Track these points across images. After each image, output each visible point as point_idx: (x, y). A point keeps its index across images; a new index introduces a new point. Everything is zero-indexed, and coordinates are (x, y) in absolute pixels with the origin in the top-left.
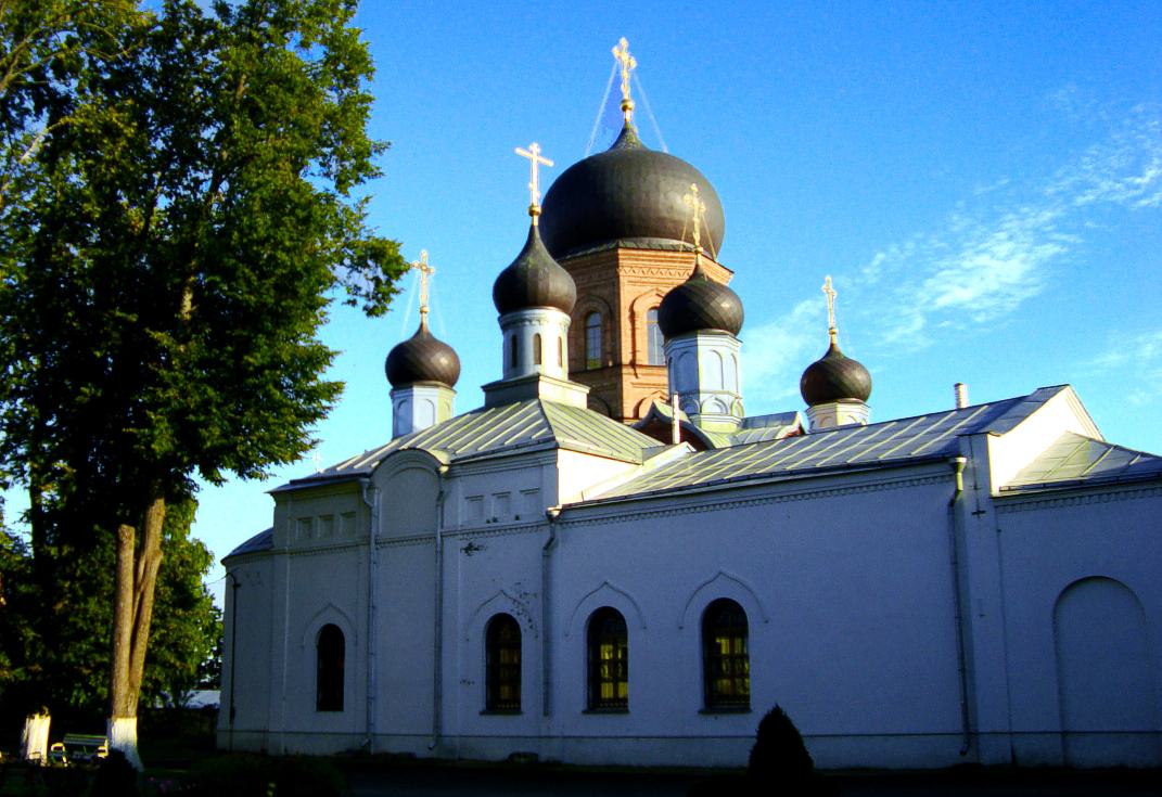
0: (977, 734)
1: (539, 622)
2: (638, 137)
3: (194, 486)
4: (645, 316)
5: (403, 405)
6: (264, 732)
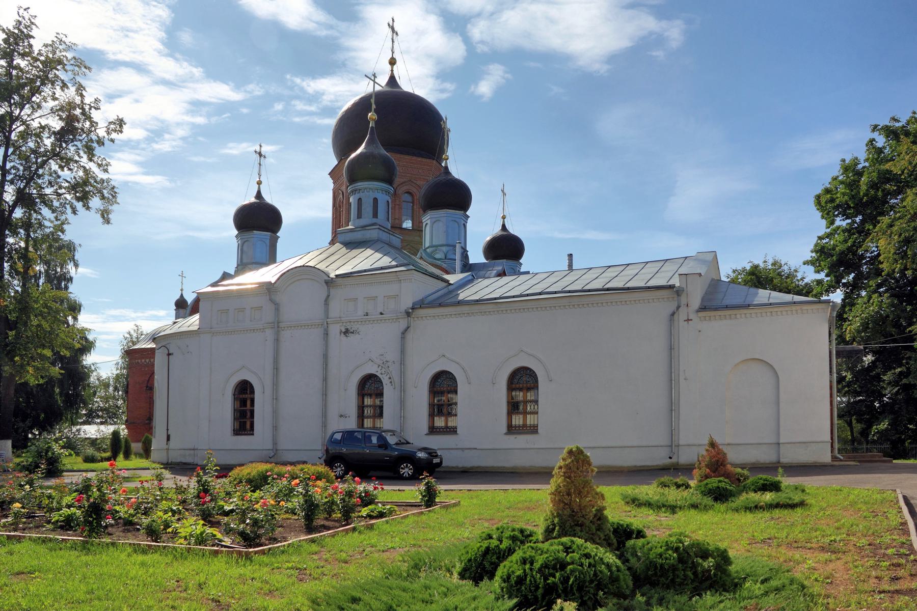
1: (396, 379)
3: (818, 272)
5: (246, 243)
6: (194, 449)
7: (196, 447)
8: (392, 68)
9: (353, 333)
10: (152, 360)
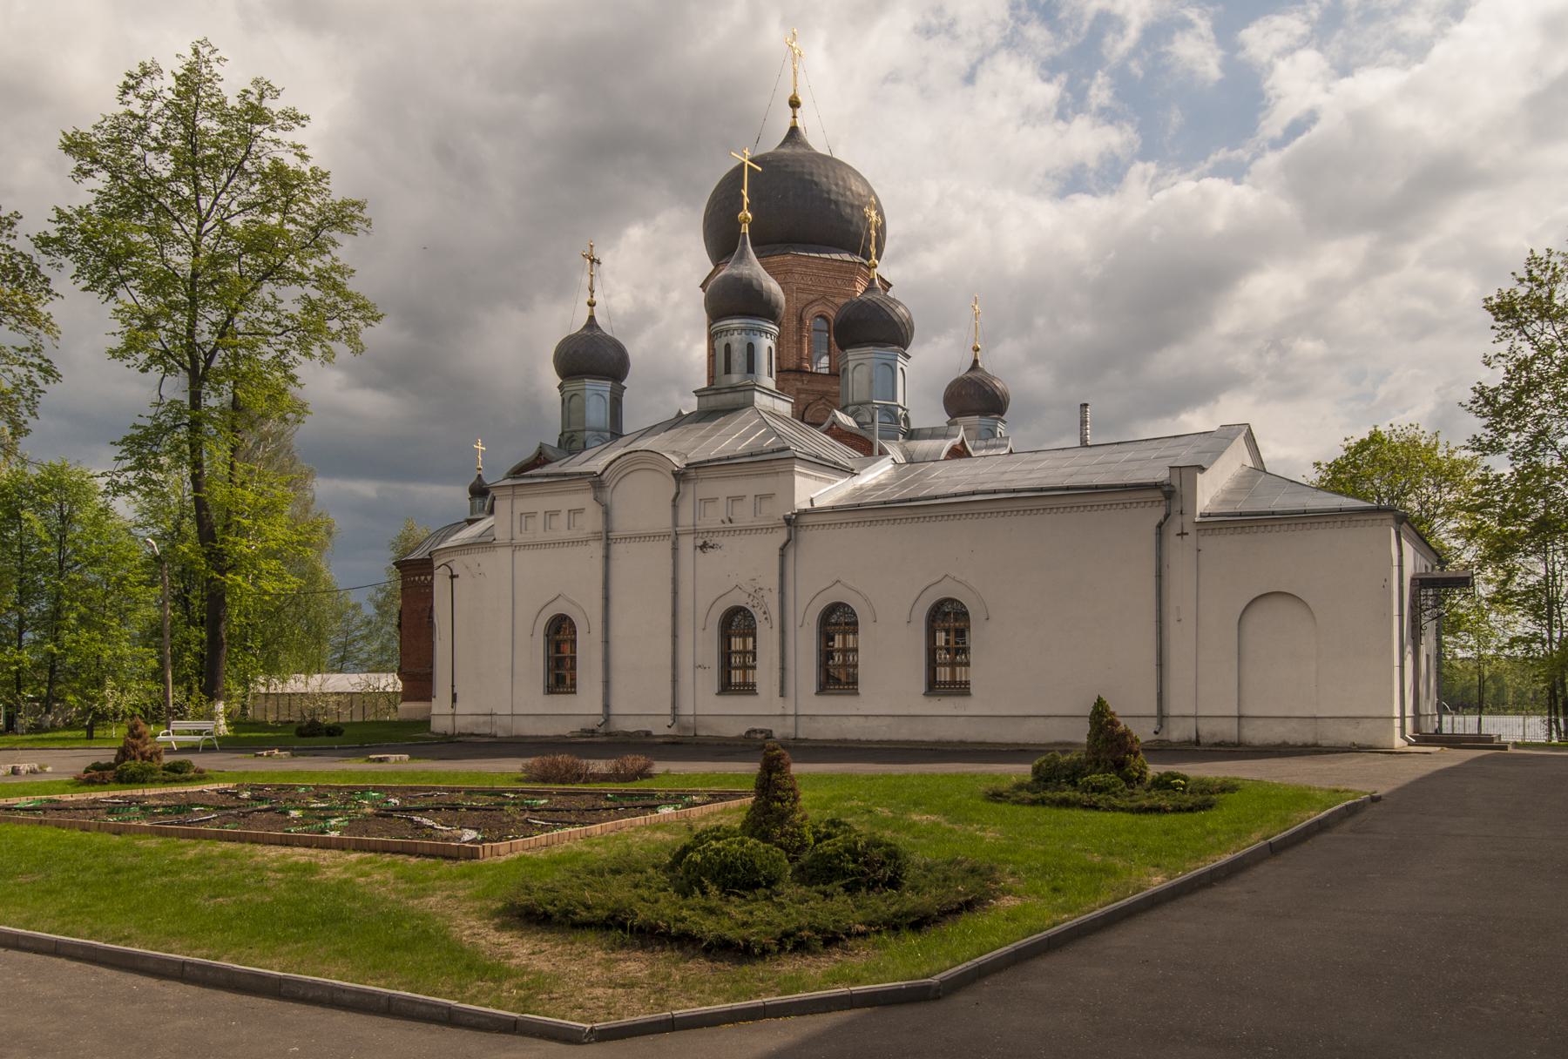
0: (1421, 715)
7: (494, 712)
8: (794, 112)
9: (712, 547)
10: (429, 578)
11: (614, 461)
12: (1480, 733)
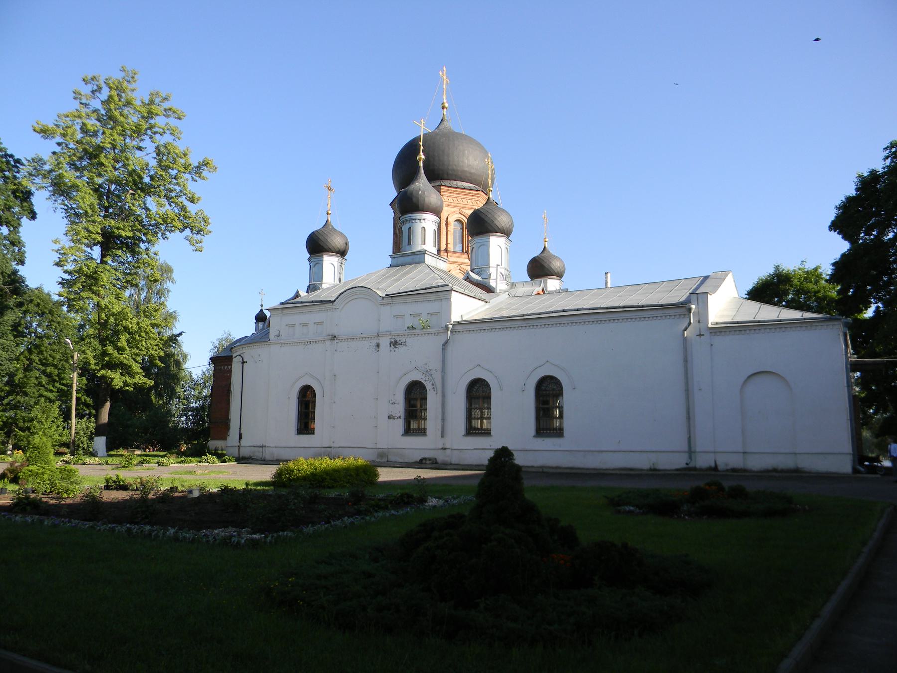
0: (695, 452)
2: (449, 124)
4: (453, 224)
5: (318, 265)
10: (229, 367)
11: (343, 293)
12: (687, 452)
